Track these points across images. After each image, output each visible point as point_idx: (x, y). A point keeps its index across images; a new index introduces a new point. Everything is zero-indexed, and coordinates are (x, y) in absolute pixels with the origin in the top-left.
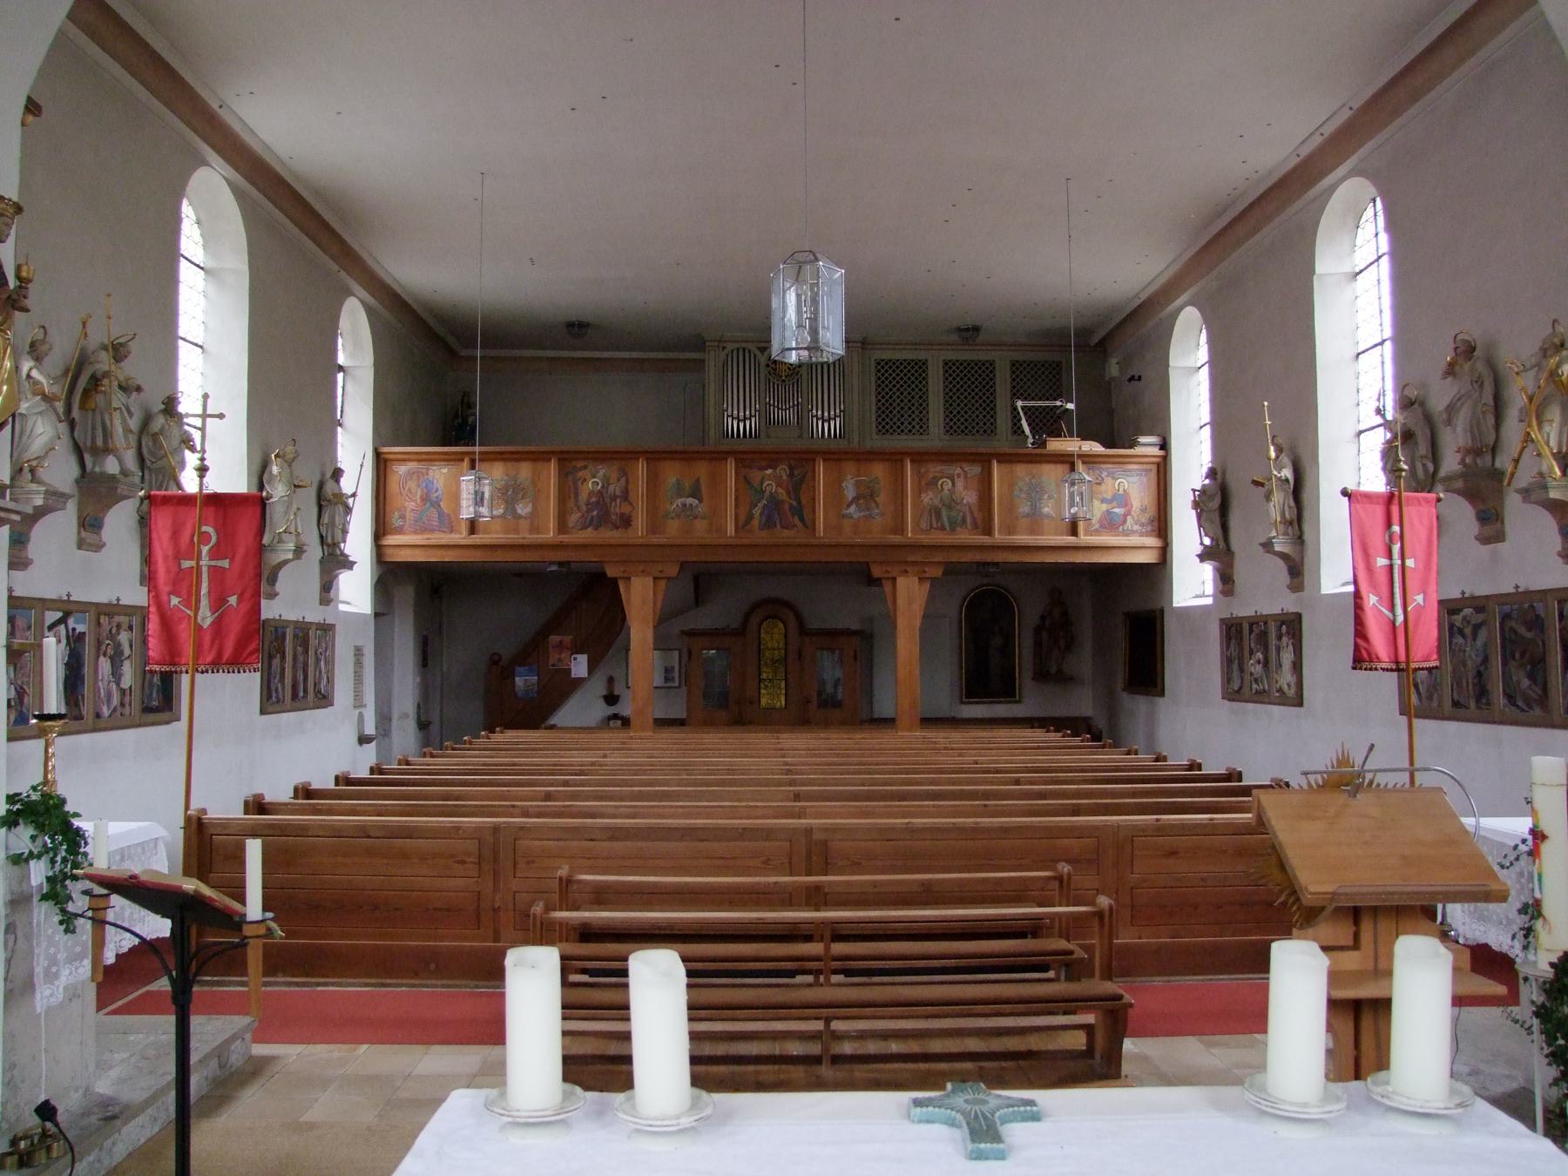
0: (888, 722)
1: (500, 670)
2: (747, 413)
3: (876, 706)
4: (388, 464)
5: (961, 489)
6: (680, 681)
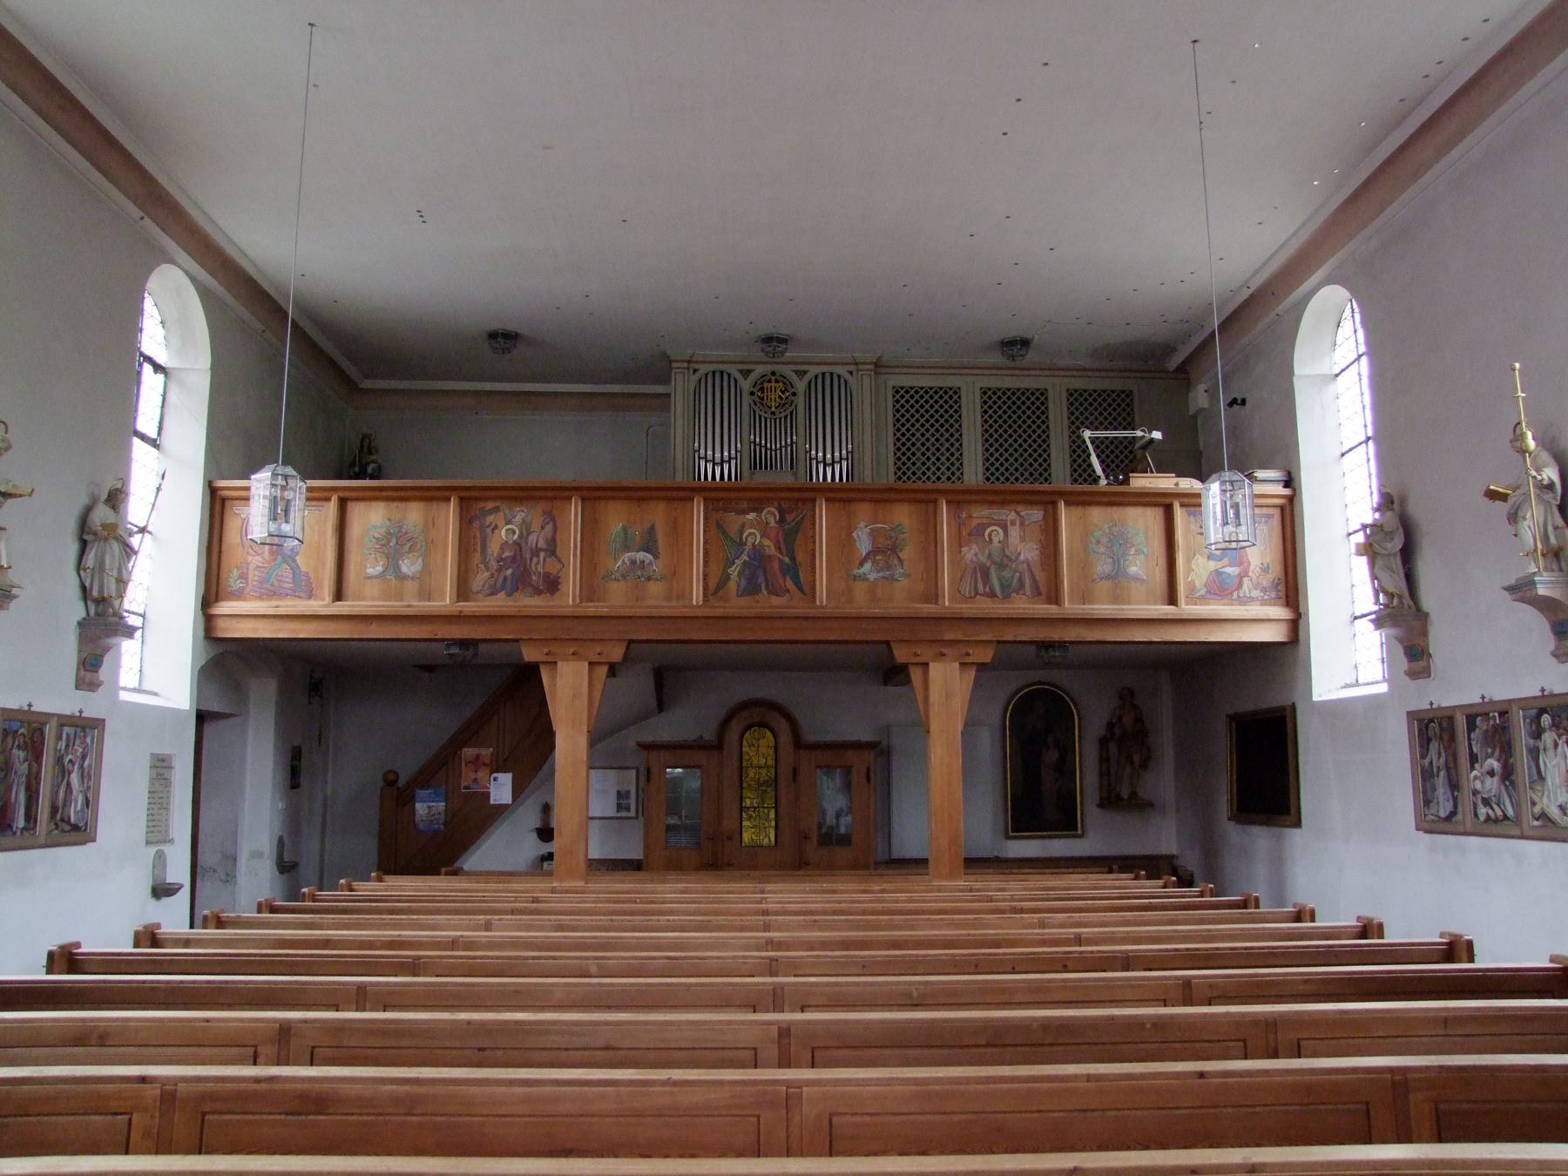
0: (918, 864)
1: (397, 794)
2: (726, 454)
3: (895, 841)
4: (228, 503)
5: (1018, 541)
6: (637, 812)
